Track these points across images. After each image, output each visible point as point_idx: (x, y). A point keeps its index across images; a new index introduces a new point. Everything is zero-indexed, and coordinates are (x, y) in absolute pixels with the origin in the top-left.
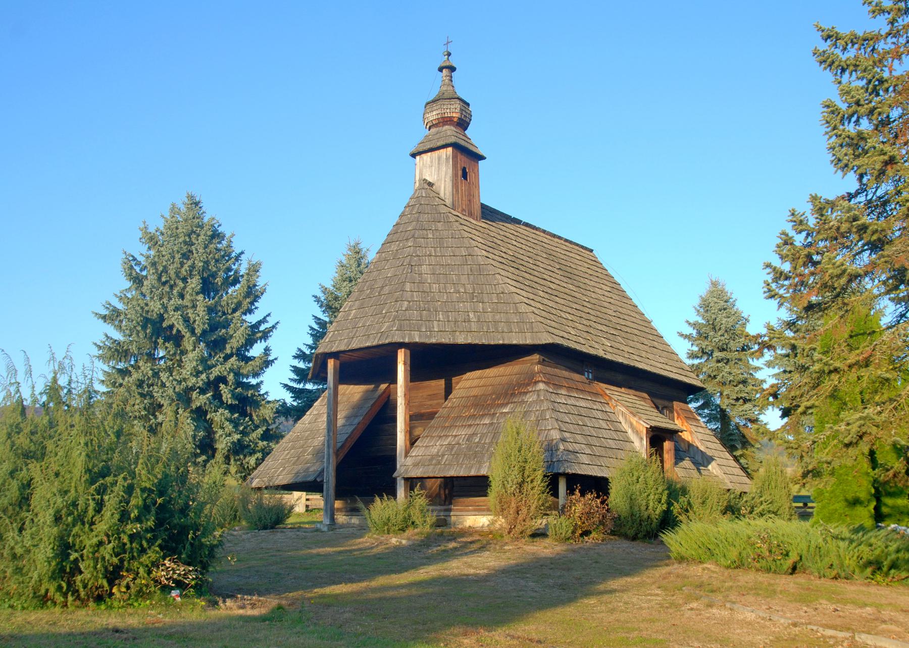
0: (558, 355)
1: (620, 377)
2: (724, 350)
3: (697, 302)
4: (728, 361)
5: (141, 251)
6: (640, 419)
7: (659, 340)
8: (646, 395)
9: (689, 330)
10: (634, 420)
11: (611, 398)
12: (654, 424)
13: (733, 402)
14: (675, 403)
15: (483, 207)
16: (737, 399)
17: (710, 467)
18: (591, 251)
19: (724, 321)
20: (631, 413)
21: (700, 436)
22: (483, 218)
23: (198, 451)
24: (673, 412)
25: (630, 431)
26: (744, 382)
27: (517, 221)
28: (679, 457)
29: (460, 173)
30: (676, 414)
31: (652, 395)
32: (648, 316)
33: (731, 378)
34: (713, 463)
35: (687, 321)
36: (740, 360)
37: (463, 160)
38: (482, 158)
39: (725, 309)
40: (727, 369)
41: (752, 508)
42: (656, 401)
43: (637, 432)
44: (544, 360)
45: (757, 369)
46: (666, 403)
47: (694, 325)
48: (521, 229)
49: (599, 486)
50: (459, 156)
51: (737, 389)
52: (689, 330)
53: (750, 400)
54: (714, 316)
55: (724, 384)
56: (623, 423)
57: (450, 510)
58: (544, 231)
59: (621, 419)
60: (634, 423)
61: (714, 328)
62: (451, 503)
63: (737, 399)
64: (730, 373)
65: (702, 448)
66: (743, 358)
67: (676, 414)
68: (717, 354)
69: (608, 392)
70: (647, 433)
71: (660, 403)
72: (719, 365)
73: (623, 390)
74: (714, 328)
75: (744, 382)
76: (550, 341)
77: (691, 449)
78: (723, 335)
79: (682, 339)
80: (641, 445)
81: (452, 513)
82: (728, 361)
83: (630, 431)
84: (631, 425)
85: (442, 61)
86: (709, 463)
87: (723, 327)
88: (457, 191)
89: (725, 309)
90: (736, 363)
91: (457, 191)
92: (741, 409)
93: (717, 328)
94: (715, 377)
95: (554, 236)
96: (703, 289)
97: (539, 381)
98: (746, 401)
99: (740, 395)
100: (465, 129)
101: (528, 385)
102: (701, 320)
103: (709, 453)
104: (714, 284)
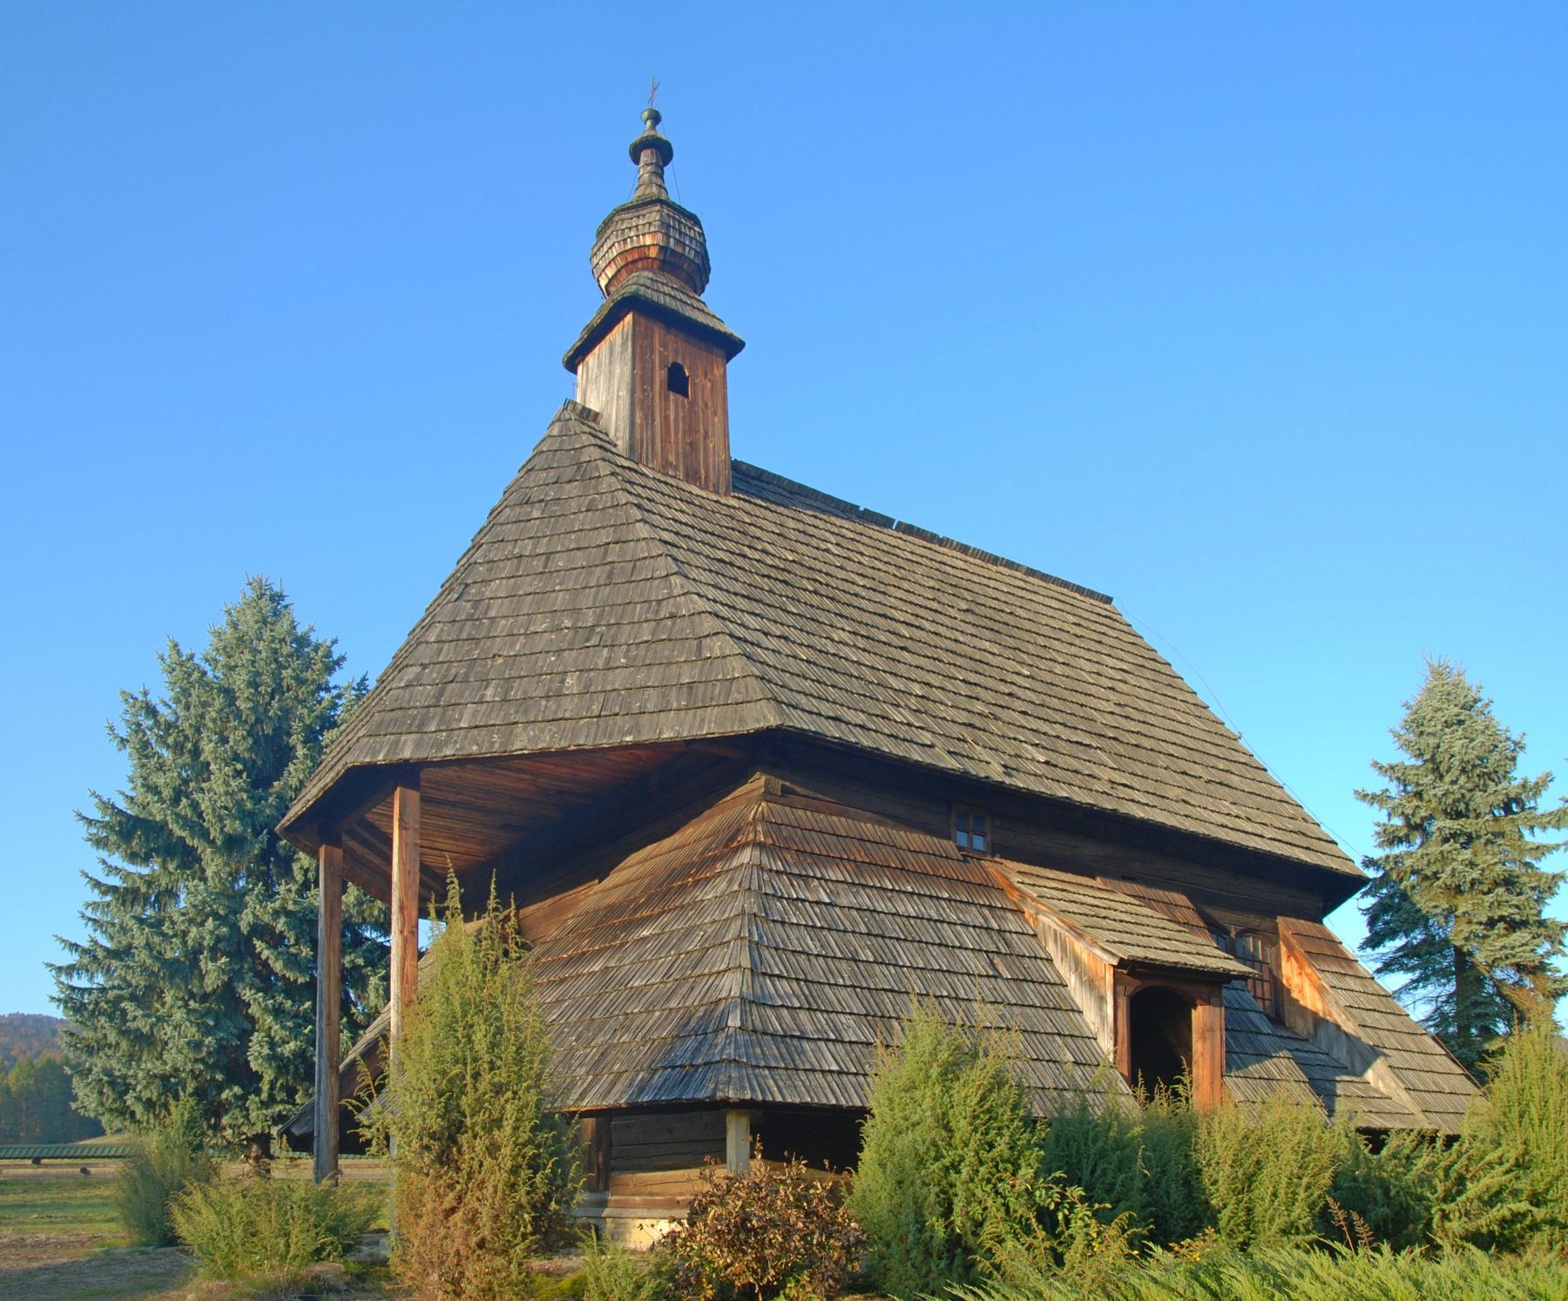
0: (789, 754)
1: (1090, 850)
2: (1459, 815)
3: (1399, 717)
4: (1470, 839)
5: (162, 693)
6: (1094, 943)
7: (1259, 775)
8: (1181, 899)
9: (1379, 783)
10: (1079, 947)
11: (1023, 895)
12: (1126, 952)
13: (1480, 930)
14: (1280, 919)
15: (738, 468)
16: (1491, 923)
17: (1370, 1075)
18: (1108, 600)
19: (1455, 745)
20: (1071, 928)
21: (1344, 999)
22: (735, 488)
23: (219, 1077)
24: (1275, 944)
25: (1072, 980)
26: (1509, 882)
27: (884, 522)
28: (1241, 1050)
29: (660, 376)
30: (1283, 949)
31: (1200, 899)
32: (1231, 726)
33: (1475, 874)
34: (1379, 1065)
35: (1375, 764)
36: (1501, 834)
37: (668, 348)
38: (730, 346)
39: (1460, 722)
40: (1467, 854)
41: (1461, 1181)
42: (1219, 915)
43: (1091, 984)
44: (785, 791)
45: (1541, 850)
46: (1253, 921)
47: (1390, 770)
48: (889, 537)
49: (826, 1136)
50: (658, 333)
51: (1489, 898)
52: (1379, 783)
53: (1524, 924)
54: (1432, 741)
55: (1458, 890)
56: (1057, 962)
57: (603, 1204)
58: (964, 549)
59: (1052, 949)
60: (1085, 957)
61: (1436, 770)
62: (607, 1188)
63: (1491, 923)
64: (1472, 865)
65: (1349, 1027)
66: (1507, 828)
67: (1283, 949)
68: (1442, 824)
69: (1015, 879)
70: (1117, 981)
71: (1231, 920)
72: (1446, 847)
73: (1098, 882)
74: (1436, 770)
75: (1509, 882)
76: (772, 720)
77: (1322, 1033)
78: (1453, 783)
79: (1364, 805)
80: (1100, 1021)
81: (607, 1212)
82: (1470, 839)
83: (1072, 980)
84: (1077, 962)
85: (644, 130)
86: (1367, 1064)
87: (1456, 762)
88: (649, 416)
89: (1460, 722)
90: (1488, 842)
91: (649, 416)
92: (1498, 944)
93: (1443, 768)
94: (1436, 876)
95: (995, 560)
96: (1412, 686)
97: (746, 844)
98: (1513, 926)
99: (1496, 914)
100: (700, 289)
101: (715, 859)
102: (1408, 760)
103: (1367, 1038)
104: (1438, 673)
